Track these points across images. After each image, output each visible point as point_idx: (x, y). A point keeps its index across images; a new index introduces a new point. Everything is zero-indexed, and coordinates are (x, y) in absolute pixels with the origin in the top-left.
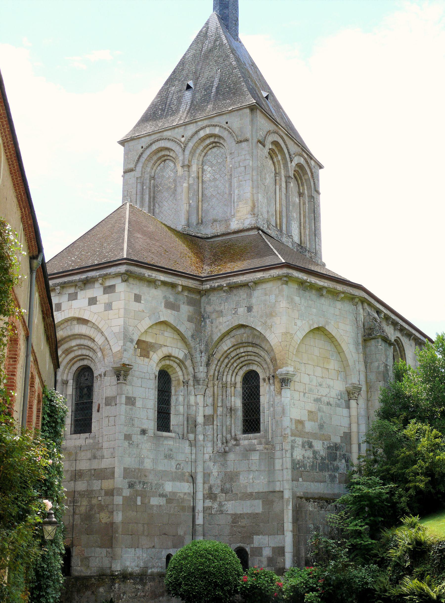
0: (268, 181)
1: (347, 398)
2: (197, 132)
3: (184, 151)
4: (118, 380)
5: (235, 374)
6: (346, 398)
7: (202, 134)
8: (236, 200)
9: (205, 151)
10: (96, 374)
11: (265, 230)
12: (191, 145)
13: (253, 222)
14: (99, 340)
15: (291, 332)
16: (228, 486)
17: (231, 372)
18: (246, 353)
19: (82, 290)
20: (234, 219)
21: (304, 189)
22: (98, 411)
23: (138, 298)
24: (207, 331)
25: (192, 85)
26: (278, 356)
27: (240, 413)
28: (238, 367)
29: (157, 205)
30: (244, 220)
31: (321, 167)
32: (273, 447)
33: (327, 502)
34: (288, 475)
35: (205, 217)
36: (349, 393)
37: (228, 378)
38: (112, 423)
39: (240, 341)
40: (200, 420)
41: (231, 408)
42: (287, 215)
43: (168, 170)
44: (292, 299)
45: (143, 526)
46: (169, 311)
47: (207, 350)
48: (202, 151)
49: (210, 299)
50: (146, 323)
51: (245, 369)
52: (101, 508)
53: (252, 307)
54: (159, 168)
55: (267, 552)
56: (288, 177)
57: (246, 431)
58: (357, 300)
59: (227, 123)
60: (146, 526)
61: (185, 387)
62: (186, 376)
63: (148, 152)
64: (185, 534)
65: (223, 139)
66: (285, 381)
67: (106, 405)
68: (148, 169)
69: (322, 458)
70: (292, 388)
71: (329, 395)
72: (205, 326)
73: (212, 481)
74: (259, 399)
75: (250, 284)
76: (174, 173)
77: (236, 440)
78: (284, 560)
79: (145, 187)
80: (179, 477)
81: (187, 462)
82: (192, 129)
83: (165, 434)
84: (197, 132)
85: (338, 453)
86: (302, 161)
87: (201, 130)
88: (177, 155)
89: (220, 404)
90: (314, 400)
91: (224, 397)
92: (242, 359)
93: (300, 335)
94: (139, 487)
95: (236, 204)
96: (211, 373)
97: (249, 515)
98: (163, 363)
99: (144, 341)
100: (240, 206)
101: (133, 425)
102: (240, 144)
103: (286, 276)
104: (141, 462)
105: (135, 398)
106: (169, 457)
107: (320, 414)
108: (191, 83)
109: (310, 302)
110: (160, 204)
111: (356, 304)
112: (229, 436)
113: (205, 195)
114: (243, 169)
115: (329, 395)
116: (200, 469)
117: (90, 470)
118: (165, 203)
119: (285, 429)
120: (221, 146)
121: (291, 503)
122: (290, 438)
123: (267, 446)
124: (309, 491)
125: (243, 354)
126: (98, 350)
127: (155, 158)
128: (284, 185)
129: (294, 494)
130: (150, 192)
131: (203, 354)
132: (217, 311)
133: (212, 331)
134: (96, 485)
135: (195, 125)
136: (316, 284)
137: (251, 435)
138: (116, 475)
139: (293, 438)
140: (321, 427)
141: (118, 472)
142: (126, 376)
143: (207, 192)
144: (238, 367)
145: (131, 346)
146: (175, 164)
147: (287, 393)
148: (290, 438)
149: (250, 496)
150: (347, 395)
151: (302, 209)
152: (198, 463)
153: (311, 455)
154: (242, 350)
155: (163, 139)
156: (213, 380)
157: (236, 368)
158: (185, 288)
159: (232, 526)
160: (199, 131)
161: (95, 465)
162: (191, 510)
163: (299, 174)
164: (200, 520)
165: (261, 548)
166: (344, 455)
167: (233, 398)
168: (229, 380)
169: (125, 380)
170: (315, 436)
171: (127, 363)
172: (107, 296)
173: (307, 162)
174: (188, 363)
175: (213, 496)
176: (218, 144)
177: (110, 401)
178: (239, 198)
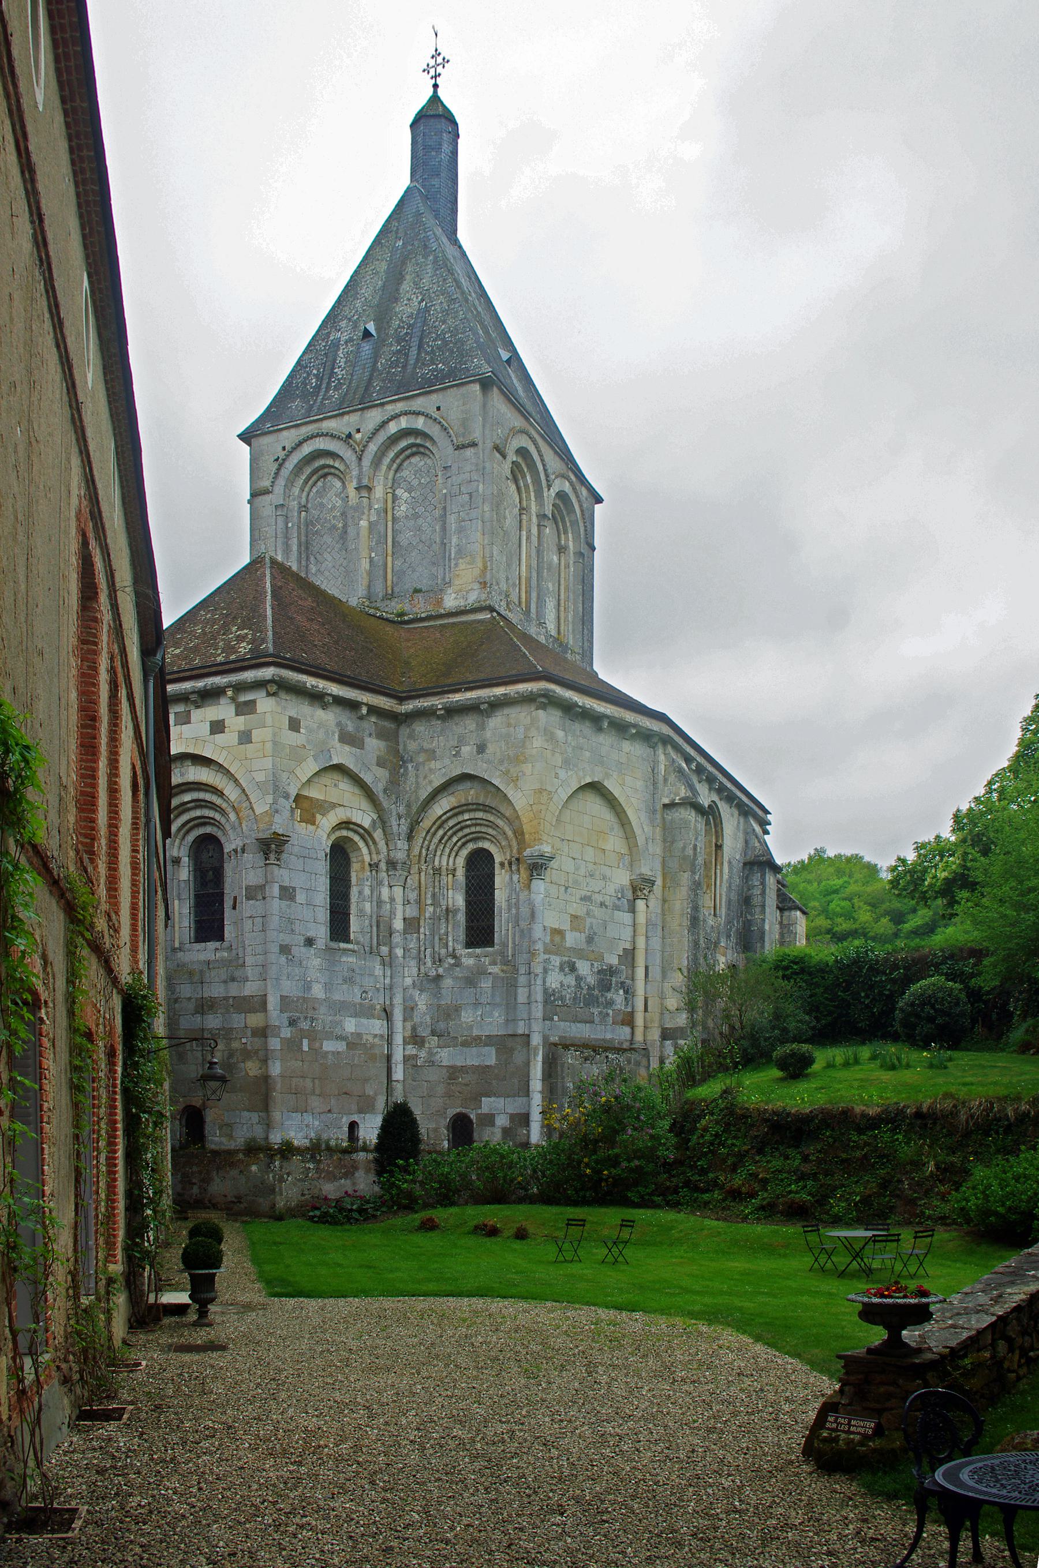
0: (508, 521)
1: (631, 898)
2: (384, 424)
3: (360, 459)
4: (266, 859)
5: (453, 854)
6: (629, 895)
7: (393, 428)
8: (453, 555)
9: (398, 461)
10: (228, 848)
11: (503, 613)
12: (373, 448)
13: (484, 596)
14: (231, 792)
15: (549, 788)
16: (442, 1025)
17: (447, 850)
18: (474, 822)
19: (198, 707)
20: (450, 591)
21: (567, 539)
22: (234, 908)
23: (294, 725)
24: (409, 783)
25: (373, 332)
26: (526, 828)
27: (461, 917)
28: (460, 843)
29: (312, 558)
30: (467, 592)
31: (599, 500)
32: (516, 970)
33: (594, 1051)
34: (538, 1011)
35: (397, 584)
36: (634, 889)
37: (442, 861)
38: (258, 927)
39: (463, 801)
40: (398, 924)
41: (447, 909)
42: (538, 585)
43: (331, 494)
44: (552, 734)
45: (313, 1081)
46: (347, 748)
47: (408, 814)
48: (393, 461)
49: (414, 730)
50: (311, 767)
51: (471, 846)
52: (247, 1054)
53: (485, 745)
54: (315, 490)
55: (502, 1121)
56: (542, 516)
57: (470, 944)
58: (655, 739)
59: (438, 409)
60: (317, 1081)
61: (374, 872)
62: (374, 856)
64: (376, 1094)
65: (431, 439)
66: (537, 867)
67: (248, 899)
68: (296, 491)
69: (589, 988)
70: (548, 879)
71: (603, 891)
72: (406, 774)
73: (417, 1020)
74: (493, 894)
75: (482, 707)
76: (343, 500)
77: (454, 957)
78: (529, 1131)
79: (290, 525)
80: (363, 1011)
81: (378, 990)
82: (375, 417)
83: (343, 945)
84: (384, 424)
85: (614, 979)
86: (567, 487)
87: (391, 420)
88: (347, 466)
89: (429, 902)
90: (581, 899)
91: (437, 890)
92: (467, 831)
93: (564, 794)
94: (305, 1025)
95: (453, 562)
96: (416, 851)
97: (476, 1069)
98: (338, 834)
99: (306, 797)
100: (462, 567)
101: (292, 930)
102: (462, 451)
103: (544, 696)
104: (307, 987)
105: (294, 889)
106: (349, 981)
107: (589, 920)
108: (371, 327)
109: (581, 740)
110: (318, 556)
111: (653, 747)
112: (443, 951)
113: (399, 543)
114: (466, 497)
115: (603, 891)
116: (398, 1000)
117: (226, 998)
118: (326, 555)
119: (534, 942)
120: (427, 452)
121: (541, 1053)
122: (542, 957)
123: (505, 968)
124: (567, 1035)
125: (468, 823)
126: (229, 810)
127: (308, 470)
128: (534, 530)
129: (545, 1038)
130: (299, 534)
131: (403, 820)
132: (426, 751)
133: (417, 783)
134: (237, 1020)
135: (380, 409)
136: (592, 709)
137: (478, 951)
138: (270, 1006)
139: (547, 956)
140: (590, 940)
141: (273, 1002)
142: (279, 853)
143: (401, 538)
144: (460, 843)
145: (287, 804)
146: (343, 483)
147: (539, 886)
148: (542, 957)
149: (478, 1041)
150: (631, 892)
151: (562, 575)
152: (395, 990)
153: (573, 983)
154: (466, 816)
155: (322, 435)
156: (419, 862)
157: (455, 844)
158: (373, 710)
159: (449, 1084)
160: (387, 422)
161: (234, 990)
162: (385, 1060)
163: (560, 511)
164: (398, 1074)
165: (493, 1115)
166: (622, 983)
167: (450, 892)
168: (444, 863)
169: (278, 860)
170: (581, 954)
171: (280, 832)
172: (242, 718)
173: (574, 489)
174: (378, 835)
175: (418, 1039)
176: (422, 450)
177: (255, 893)
178: (460, 551)
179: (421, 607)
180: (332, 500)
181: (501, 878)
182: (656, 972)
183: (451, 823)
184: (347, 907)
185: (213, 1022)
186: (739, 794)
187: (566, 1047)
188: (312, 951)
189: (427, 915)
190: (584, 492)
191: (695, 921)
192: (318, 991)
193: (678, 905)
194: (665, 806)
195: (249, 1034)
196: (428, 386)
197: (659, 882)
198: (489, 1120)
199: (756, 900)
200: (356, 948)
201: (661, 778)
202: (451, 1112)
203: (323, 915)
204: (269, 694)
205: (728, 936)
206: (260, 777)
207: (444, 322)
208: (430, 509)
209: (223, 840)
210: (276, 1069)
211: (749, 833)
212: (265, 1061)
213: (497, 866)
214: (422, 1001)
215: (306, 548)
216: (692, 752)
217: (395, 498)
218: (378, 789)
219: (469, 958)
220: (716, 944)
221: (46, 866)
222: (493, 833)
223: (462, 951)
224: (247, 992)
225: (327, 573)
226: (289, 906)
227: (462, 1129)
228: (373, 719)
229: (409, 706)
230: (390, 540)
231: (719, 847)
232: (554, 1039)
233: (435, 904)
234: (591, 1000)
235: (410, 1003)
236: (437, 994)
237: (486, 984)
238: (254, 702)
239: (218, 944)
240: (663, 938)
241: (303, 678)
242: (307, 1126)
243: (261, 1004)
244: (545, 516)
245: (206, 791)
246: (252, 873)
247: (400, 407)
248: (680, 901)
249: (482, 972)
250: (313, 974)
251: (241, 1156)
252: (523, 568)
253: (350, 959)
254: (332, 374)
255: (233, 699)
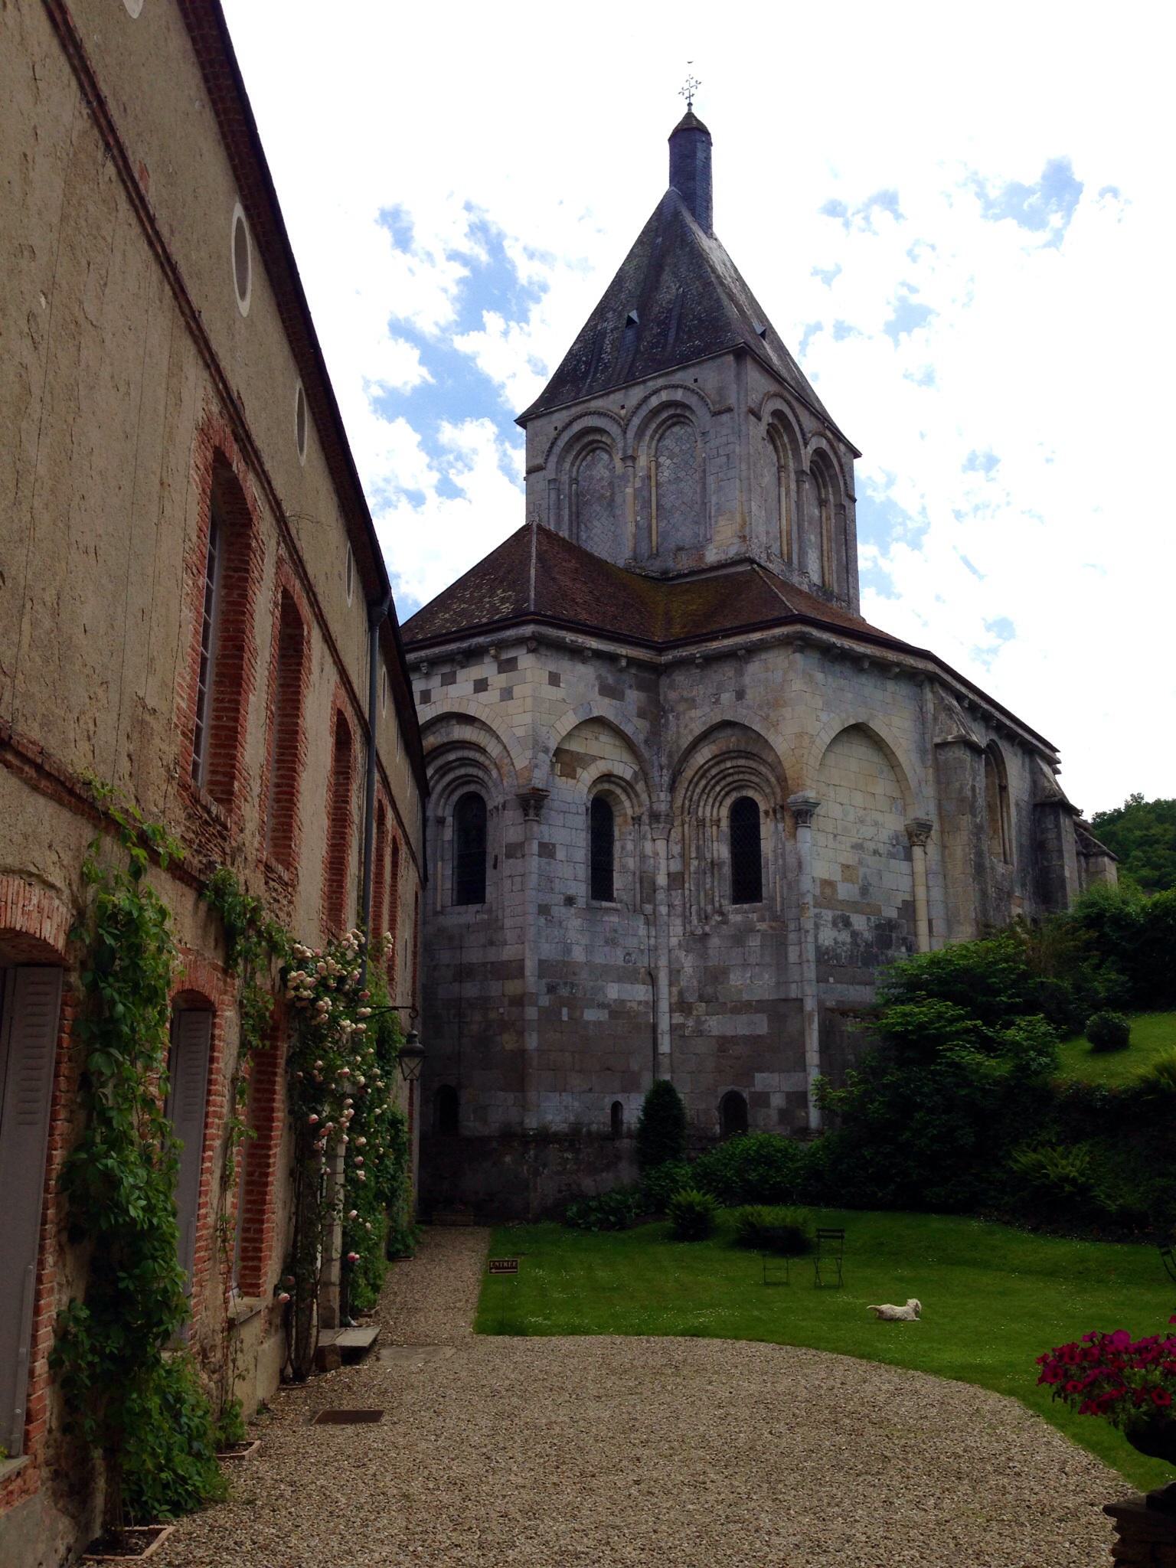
2: (646, 399)
4: (526, 815)
6: (905, 840)
7: (654, 401)
10: (490, 806)
13: (744, 549)
14: (494, 749)
16: (710, 990)
17: (711, 800)
19: (463, 667)
20: (711, 547)
21: (827, 493)
22: (495, 867)
23: (554, 680)
26: (789, 773)
27: (727, 870)
32: (784, 926)
34: (810, 972)
36: (910, 835)
37: (706, 811)
38: (518, 887)
40: (662, 880)
46: (607, 700)
50: (570, 721)
51: (735, 795)
55: (777, 1101)
56: (800, 473)
57: (737, 899)
58: (922, 677)
59: (696, 381)
63: (566, 437)
66: (803, 814)
68: (567, 466)
72: (666, 725)
75: (740, 653)
76: (610, 470)
77: (722, 914)
80: (627, 975)
81: (642, 951)
82: (637, 393)
83: (605, 904)
84: (646, 399)
86: (824, 444)
89: (693, 855)
92: (729, 779)
94: (564, 992)
96: (679, 803)
97: (747, 1039)
98: (600, 787)
104: (567, 950)
105: (554, 845)
106: (612, 942)
107: (862, 871)
108: (634, 315)
111: (920, 686)
112: (709, 908)
114: (724, 459)
116: (663, 962)
117: (484, 964)
118: (596, 523)
121: (816, 1019)
122: (812, 911)
126: (492, 767)
129: (821, 1004)
131: (665, 771)
132: (686, 700)
133: (678, 732)
134: (495, 988)
136: (851, 650)
137: (746, 906)
138: (528, 973)
139: (817, 910)
140: (864, 891)
141: (530, 966)
145: (545, 759)
147: (804, 834)
153: (849, 940)
154: (729, 764)
155: (590, 414)
158: (632, 661)
161: (492, 955)
164: (665, 1047)
166: (904, 939)
168: (708, 814)
170: (855, 906)
171: (540, 786)
174: (640, 787)
179: (685, 563)
180: (600, 471)
181: (766, 828)
182: (939, 926)
183: (714, 772)
184: (610, 863)
185: (471, 990)
186: (1020, 731)
187: (844, 1014)
188: (573, 911)
189: (692, 869)
190: (842, 448)
191: (980, 869)
192: (578, 955)
193: (959, 852)
194: (937, 746)
195: (506, 1003)
196: (684, 362)
197: (936, 826)
198: (763, 1099)
199: (1052, 844)
200: (619, 906)
201: (930, 716)
202: (723, 1090)
203: (583, 872)
204: (530, 651)
205: (1023, 885)
206: (520, 732)
207: (699, 304)
208: (690, 472)
209: (486, 797)
210: (532, 1041)
211: (1036, 775)
212: (521, 1034)
213: (762, 814)
214: (688, 963)
215: (577, 517)
216: (963, 690)
217: (658, 465)
218: (639, 739)
219: (736, 915)
220: (1010, 894)
221: (71, 792)
222: (757, 780)
223: (729, 907)
224: (505, 957)
225: (596, 539)
226: (549, 864)
227: (735, 1111)
228: (633, 671)
229: (668, 657)
230: (654, 506)
231: (1003, 789)
232: (830, 1003)
233: (700, 857)
234: (870, 959)
235: (675, 966)
236: (704, 955)
237: (754, 942)
238: (515, 658)
239: (478, 907)
240: (946, 887)
241: (562, 633)
242: (566, 1107)
243: (517, 970)
244: (803, 472)
245: (470, 749)
246: (512, 830)
247: (661, 382)
248: (960, 846)
249: (750, 930)
250: (575, 937)
251: (495, 1144)
252: (784, 522)
253: (612, 919)
254: (600, 359)
255: (496, 657)
